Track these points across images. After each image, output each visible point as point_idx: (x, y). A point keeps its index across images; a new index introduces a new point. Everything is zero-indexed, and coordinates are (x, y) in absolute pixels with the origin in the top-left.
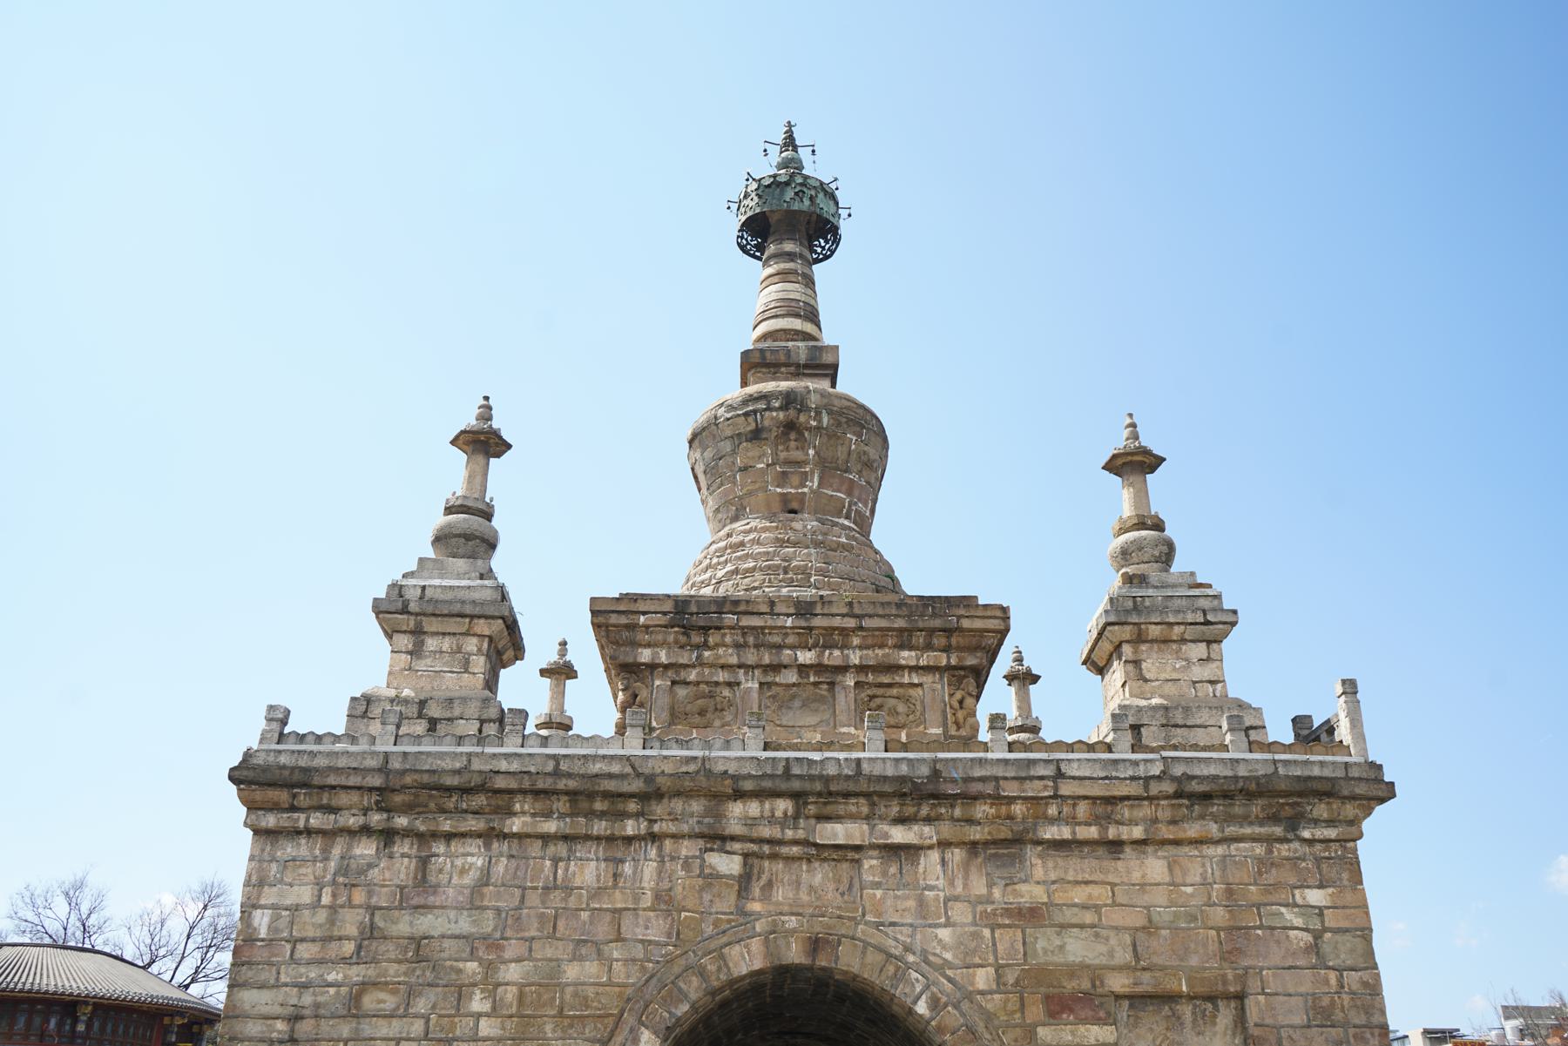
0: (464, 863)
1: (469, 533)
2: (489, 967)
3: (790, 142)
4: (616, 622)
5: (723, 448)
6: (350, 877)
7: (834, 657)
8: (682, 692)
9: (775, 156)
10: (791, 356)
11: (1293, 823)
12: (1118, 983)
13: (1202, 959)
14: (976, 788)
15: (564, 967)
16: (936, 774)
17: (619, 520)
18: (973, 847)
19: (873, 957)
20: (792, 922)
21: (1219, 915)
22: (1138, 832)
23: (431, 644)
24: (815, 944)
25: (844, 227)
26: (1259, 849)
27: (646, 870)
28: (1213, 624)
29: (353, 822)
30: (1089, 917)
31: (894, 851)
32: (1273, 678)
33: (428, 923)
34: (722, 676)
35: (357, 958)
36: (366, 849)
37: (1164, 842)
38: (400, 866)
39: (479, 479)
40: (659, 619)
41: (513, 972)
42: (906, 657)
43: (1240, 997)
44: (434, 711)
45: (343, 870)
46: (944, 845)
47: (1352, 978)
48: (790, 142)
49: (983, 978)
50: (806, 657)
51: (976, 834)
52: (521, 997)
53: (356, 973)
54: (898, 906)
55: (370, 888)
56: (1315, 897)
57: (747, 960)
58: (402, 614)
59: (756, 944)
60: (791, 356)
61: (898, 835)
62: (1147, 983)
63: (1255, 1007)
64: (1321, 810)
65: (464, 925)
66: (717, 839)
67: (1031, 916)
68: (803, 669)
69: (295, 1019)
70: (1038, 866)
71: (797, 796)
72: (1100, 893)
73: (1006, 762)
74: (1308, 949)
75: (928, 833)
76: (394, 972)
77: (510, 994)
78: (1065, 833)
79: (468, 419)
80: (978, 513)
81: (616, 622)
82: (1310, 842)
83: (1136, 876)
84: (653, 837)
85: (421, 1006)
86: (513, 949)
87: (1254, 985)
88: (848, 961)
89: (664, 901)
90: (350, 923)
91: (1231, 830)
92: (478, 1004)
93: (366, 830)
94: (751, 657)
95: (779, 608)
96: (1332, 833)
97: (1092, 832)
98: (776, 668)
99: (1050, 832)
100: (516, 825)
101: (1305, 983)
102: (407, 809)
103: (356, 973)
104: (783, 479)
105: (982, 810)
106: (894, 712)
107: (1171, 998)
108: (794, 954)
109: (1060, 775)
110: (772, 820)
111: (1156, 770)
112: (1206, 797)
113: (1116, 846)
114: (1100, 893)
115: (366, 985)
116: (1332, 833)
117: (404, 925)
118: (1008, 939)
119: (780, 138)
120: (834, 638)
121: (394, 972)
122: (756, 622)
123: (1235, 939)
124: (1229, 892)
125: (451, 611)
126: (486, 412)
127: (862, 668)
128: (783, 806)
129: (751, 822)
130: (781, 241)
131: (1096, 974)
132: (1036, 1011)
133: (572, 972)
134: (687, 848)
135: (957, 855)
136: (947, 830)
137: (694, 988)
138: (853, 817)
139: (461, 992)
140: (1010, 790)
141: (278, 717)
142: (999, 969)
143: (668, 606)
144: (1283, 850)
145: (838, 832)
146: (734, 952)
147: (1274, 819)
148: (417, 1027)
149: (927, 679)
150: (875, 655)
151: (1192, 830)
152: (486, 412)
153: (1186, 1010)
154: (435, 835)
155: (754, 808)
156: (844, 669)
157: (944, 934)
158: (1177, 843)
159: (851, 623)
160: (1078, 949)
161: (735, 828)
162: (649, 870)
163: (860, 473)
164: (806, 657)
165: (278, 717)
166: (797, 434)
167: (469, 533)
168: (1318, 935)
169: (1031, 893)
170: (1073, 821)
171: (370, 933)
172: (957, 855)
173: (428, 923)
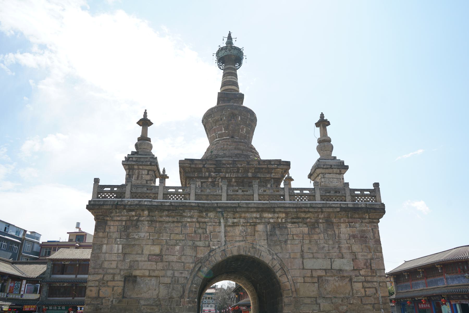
3: (230, 37)
5: (210, 120)
9: (226, 40)
10: (230, 96)
15: (108, 222)
17: (181, 143)
25: (244, 61)
28: (342, 167)
32: (356, 179)
39: (145, 132)
48: (230, 37)
60: (230, 96)
73: (289, 203)
79: (318, 119)
80: (280, 139)
119: (227, 36)
126: (322, 116)
130: (229, 64)
152: (322, 116)
163: (216, 125)
166: (230, 117)
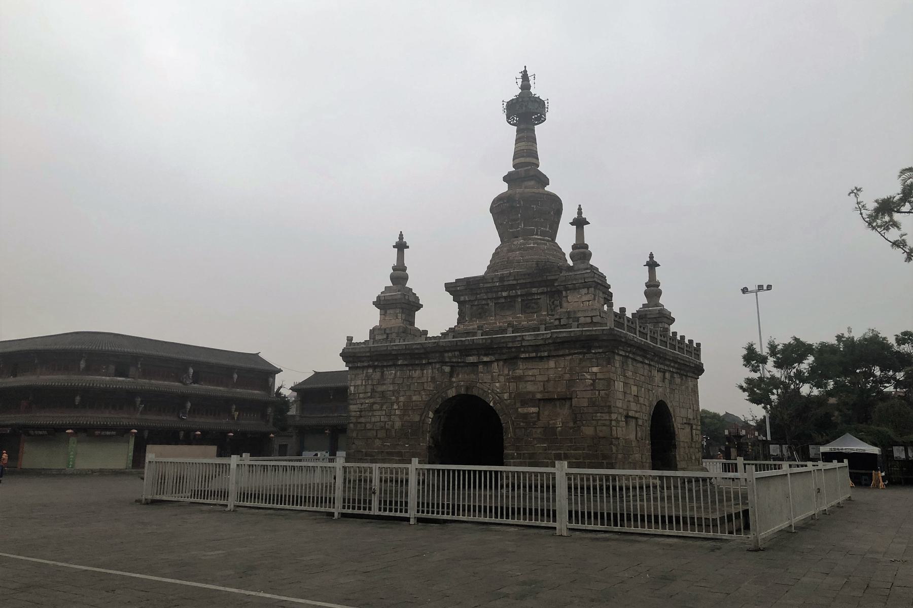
0: (391, 373)
1: (399, 275)
2: (397, 398)
3: (525, 76)
4: (460, 290)
6: (368, 378)
7: (513, 293)
8: (475, 308)
11: (589, 348)
12: (539, 396)
13: (561, 389)
14: (501, 345)
16: (492, 341)
18: (505, 361)
19: (481, 392)
20: (462, 383)
21: (567, 376)
22: (546, 354)
23: (388, 312)
24: (467, 388)
26: (581, 357)
27: (428, 372)
29: (366, 364)
30: (533, 378)
31: (485, 363)
33: (384, 388)
34: (484, 302)
35: (371, 397)
36: (370, 371)
37: (554, 356)
38: (377, 375)
40: (462, 288)
41: (402, 399)
42: (534, 290)
43: (571, 399)
44: (388, 332)
45: (366, 376)
46: (497, 360)
47: (602, 393)
49: (506, 396)
50: (505, 294)
51: (505, 357)
52: (404, 405)
53: (372, 400)
54: (487, 378)
55: (372, 380)
56: (595, 369)
57: (452, 393)
58: (381, 303)
59: (454, 389)
61: (485, 359)
62: (547, 396)
63: (574, 401)
64: (596, 344)
65: (391, 388)
66: (444, 363)
67: (519, 379)
68: (505, 297)
69: (361, 411)
70: (521, 365)
71: (459, 351)
72: (536, 372)
74: (592, 384)
75: (493, 358)
76: (378, 400)
77: (401, 404)
78: (527, 355)
81: (460, 290)
82: (595, 353)
83: (546, 367)
84: (430, 363)
85: (384, 407)
86: (401, 394)
87: (574, 395)
88: (475, 392)
89: (433, 379)
90: (369, 389)
91: (572, 351)
92: (395, 407)
93: (369, 367)
94: (490, 295)
95: (495, 280)
96: (601, 351)
97: (534, 355)
98: (498, 298)
99: (523, 356)
100: (400, 362)
101: (588, 395)
102: (377, 360)
103: (372, 400)
104: (512, 227)
105: (505, 351)
106: (533, 308)
107: (554, 399)
108: (463, 391)
109: (523, 339)
110: (455, 357)
111: (549, 336)
112: (563, 343)
113: (541, 358)
114: (536, 372)
115: (374, 403)
116: (601, 351)
117: (380, 389)
118: (513, 386)
120: (512, 287)
121: (378, 400)
122: (489, 285)
123: (571, 382)
124: (571, 369)
125: (399, 302)
127: (521, 295)
128: (457, 353)
129: (450, 358)
131: (533, 393)
132: (518, 405)
133: (414, 398)
134: (438, 366)
135: (501, 363)
136: (497, 357)
137: (440, 401)
138: (473, 355)
139: (392, 404)
140: (510, 345)
141: (350, 339)
142: (510, 394)
143: (465, 283)
144: (588, 356)
145: (472, 359)
146: (449, 391)
147: (583, 347)
148: (384, 413)
149: (542, 296)
150: (524, 291)
151: (561, 353)
153: (558, 403)
154: (384, 366)
155: (450, 354)
156: (517, 296)
157: (497, 385)
158: (558, 356)
159: (515, 282)
160: (530, 387)
161: (447, 360)
162: (430, 371)
164: (505, 294)
165: (350, 339)
167: (399, 275)
168: (594, 381)
169: (519, 372)
170: (529, 352)
171: (373, 391)
172: (501, 363)
173: (384, 388)
